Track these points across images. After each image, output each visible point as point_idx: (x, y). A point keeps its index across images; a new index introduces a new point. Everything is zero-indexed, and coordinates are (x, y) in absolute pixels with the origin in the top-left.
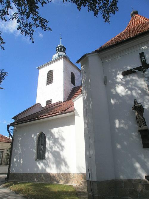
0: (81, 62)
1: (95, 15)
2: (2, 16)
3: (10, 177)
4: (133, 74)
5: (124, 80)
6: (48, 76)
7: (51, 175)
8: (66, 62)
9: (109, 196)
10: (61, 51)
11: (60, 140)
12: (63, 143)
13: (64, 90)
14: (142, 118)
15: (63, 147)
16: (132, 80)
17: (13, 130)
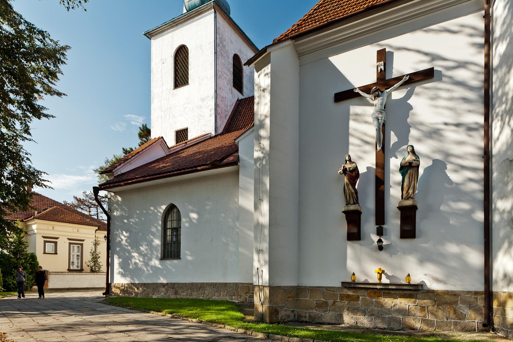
8: (222, 23)
9: (286, 308)
14: (353, 191)
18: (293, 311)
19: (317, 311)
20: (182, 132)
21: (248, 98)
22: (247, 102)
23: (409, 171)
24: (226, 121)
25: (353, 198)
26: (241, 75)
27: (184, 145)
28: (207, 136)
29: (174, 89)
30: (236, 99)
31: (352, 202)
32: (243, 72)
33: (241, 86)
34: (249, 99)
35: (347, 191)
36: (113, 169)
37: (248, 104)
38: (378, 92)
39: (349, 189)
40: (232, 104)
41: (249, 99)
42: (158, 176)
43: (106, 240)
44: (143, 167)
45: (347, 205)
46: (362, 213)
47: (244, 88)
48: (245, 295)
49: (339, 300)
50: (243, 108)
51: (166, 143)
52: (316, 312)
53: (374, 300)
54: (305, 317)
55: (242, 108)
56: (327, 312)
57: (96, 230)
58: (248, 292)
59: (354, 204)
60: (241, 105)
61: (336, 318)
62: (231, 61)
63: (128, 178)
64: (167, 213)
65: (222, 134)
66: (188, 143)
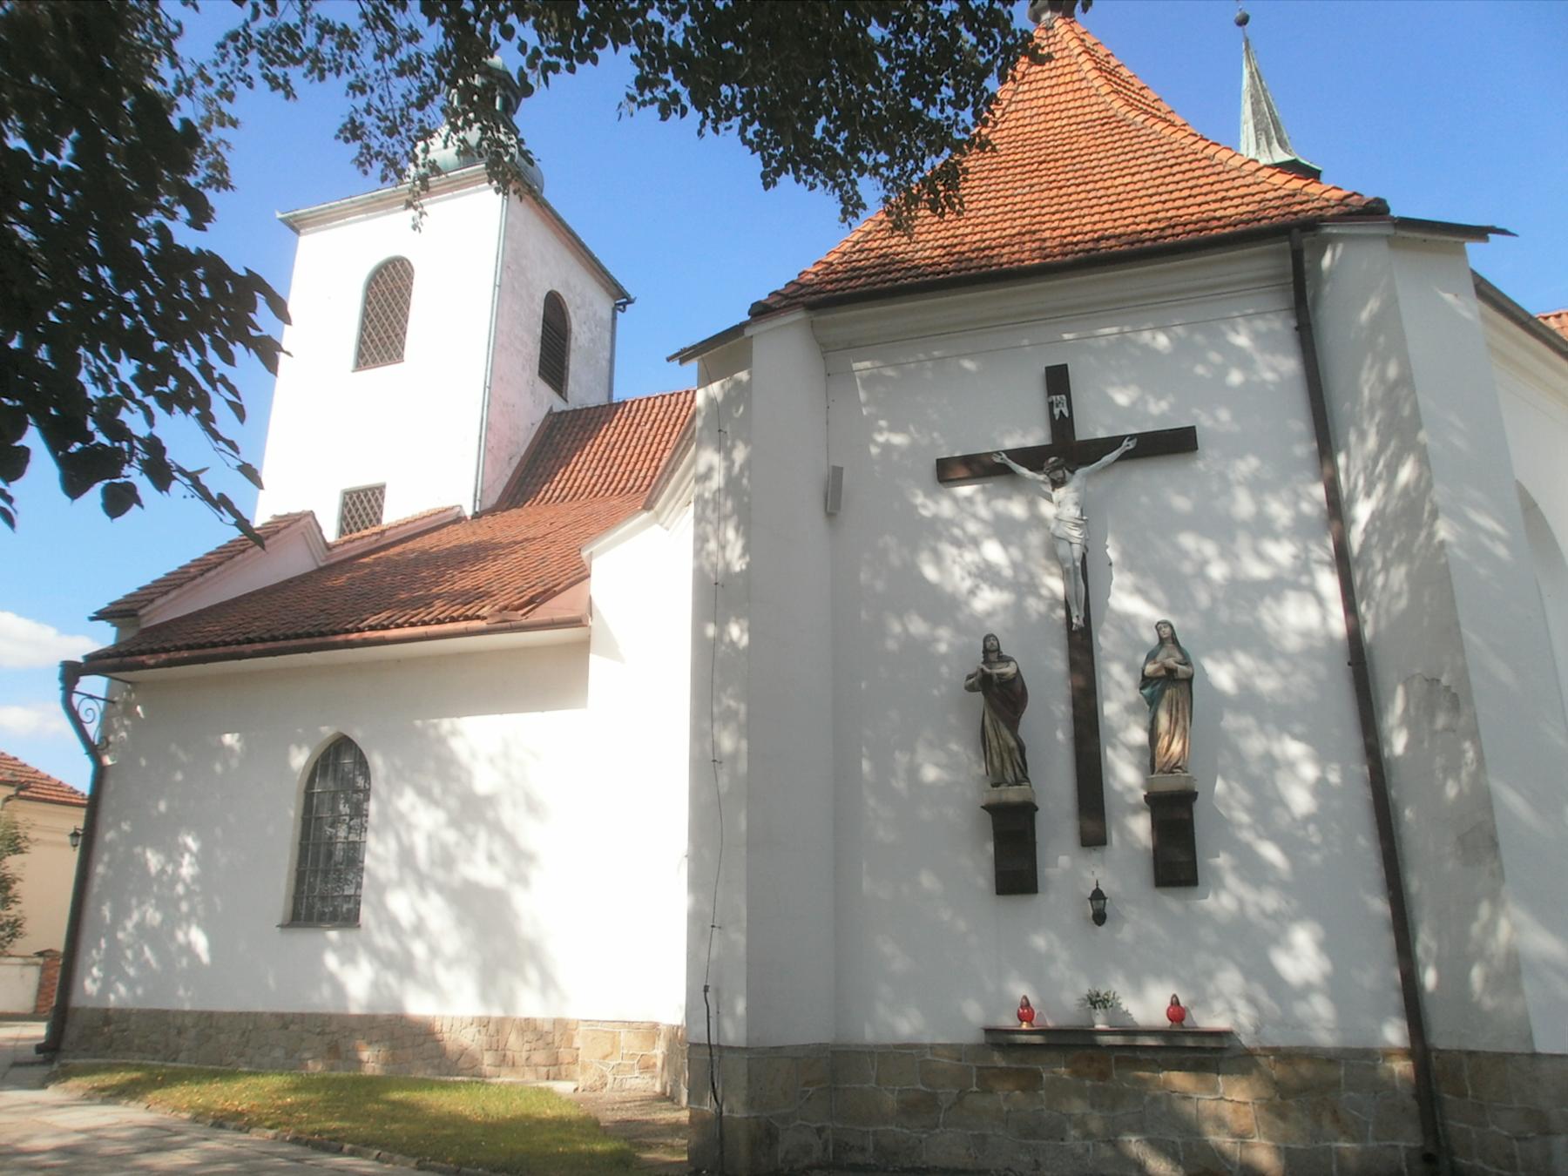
0: (699, 361)
1: (844, 220)
2: (272, 62)
3: (72, 1033)
4: (1003, 478)
6: (367, 301)
8: (523, 210)
9: (799, 1122)
11: (509, 815)
12: (529, 834)
13: (489, 428)
14: (1013, 743)
15: (521, 857)
17: (102, 703)
18: (820, 1131)
19: (902, 1127)
20: (366, 495)
21: (582, 410)
22: (580, 423)
23: (1168, 692)
24: (510, 473)
25: (1012, 763)
26: (565, 346)
27: (374, 538)
29: (353, 371)
30: (546, 410)
31: (1009, 776)
34: (587, 414)
35: (994, 744)
36: (141, 608)
37: (581, 427)
40: (533, 424)
41: (587, 414)
42: (307, 641)
43: (78, 848)
45: (994, 785)
46: (1037, 809)
48: (600, 1063)
49: (975, 1089)
51: (320, 531)
52: (899, 1130)
53: (1088, 1083)
54: (863, 1150)
56: (938, 1131)
57: (8, 799)
58: (612, 1053)
59: (1018, 783)
60: (560, 429)
61: (968, 1149)
65: (492, 511)
66: (387, 534)
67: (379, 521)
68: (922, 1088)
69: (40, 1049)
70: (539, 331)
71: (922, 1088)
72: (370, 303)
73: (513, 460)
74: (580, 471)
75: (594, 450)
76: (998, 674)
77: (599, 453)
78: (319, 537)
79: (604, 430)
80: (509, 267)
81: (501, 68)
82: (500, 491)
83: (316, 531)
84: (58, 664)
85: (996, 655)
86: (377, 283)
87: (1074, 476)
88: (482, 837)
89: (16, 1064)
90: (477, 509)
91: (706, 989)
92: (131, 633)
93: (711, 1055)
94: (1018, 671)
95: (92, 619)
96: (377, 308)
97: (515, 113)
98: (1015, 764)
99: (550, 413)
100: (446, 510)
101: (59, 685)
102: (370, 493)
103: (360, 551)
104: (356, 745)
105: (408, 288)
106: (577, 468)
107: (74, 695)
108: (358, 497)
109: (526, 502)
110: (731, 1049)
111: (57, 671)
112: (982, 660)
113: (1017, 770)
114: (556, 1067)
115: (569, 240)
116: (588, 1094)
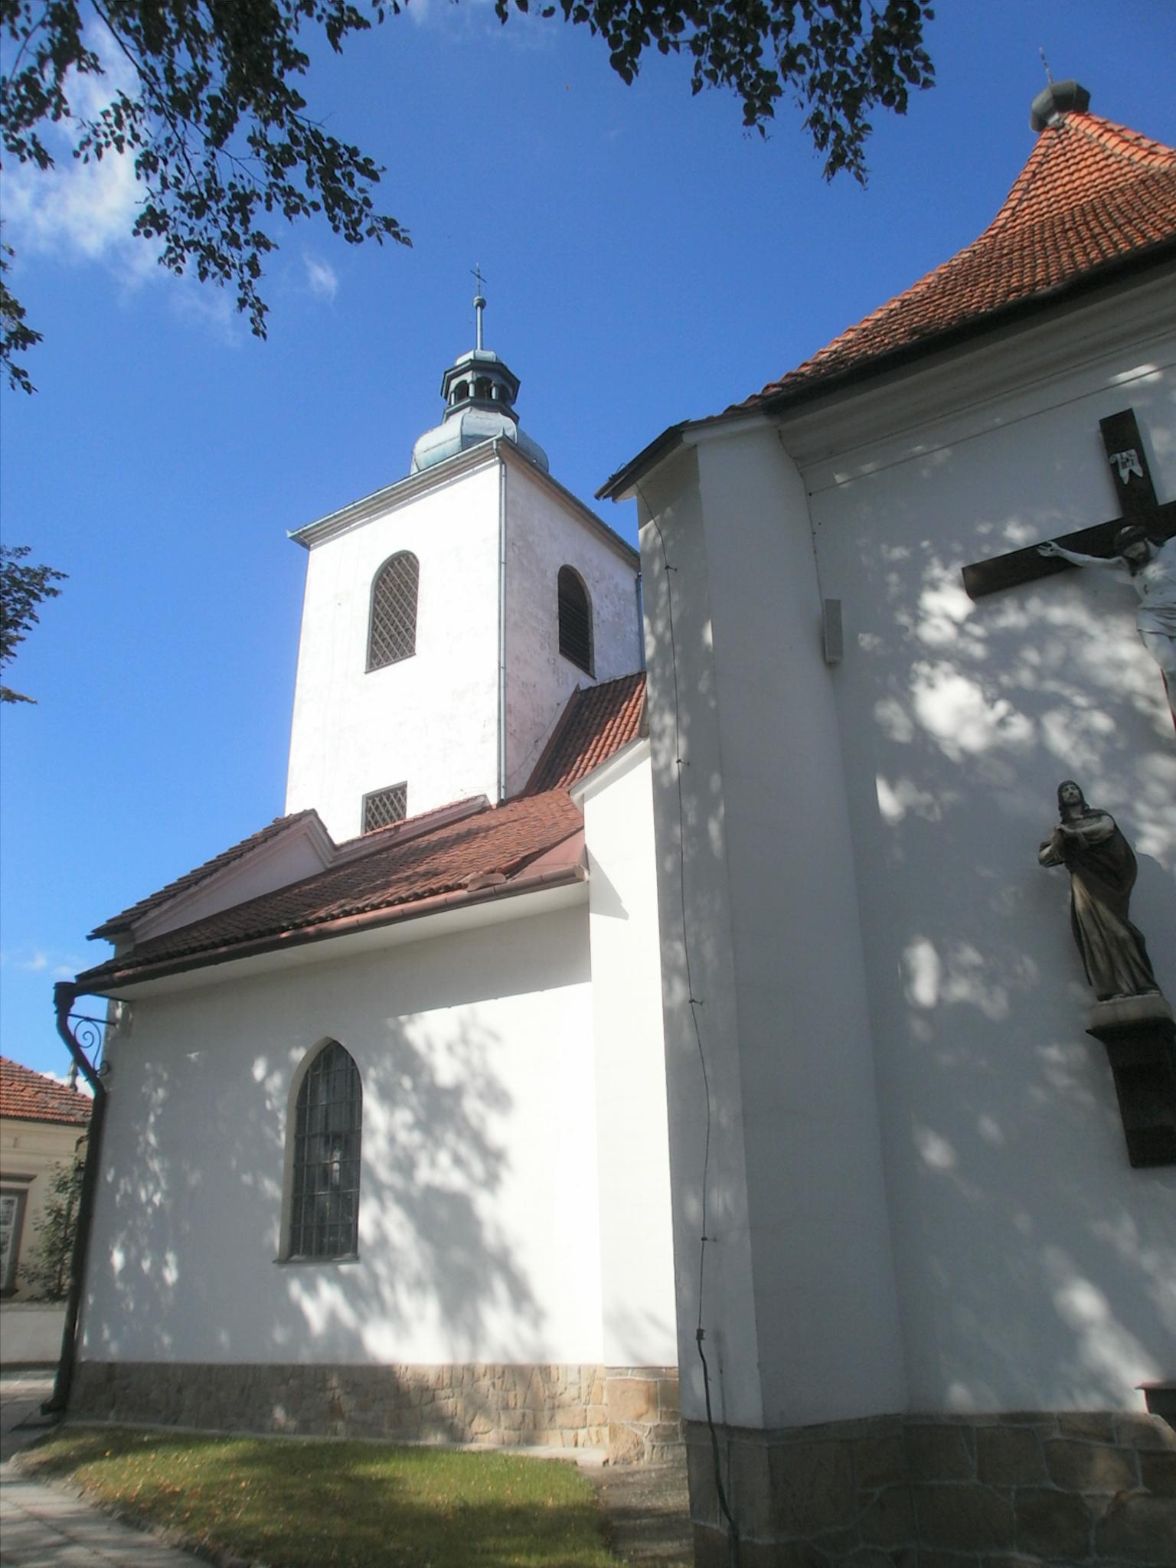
3: (78, 1390)
5: (977, 630)
6: (375, 601)
7: (406, 1379)
10: (483, 401)
12: (498, 1130)
14: (1123, 933)
16: (1041, 633)
17: (102, 1027)
20: (388, 798)
21: (610, 684)
22: (609, 697)
24: (537, 756)
25: (1127, 964)
27: (388, 834)
28: (470, 804)
29: (366, 673)
30: (572, 690)
32: (591, 614)
33: (588, 651)
34: (615, 686)
35: (1095, 937)
36: (134, 921)
37: (610, 700)
38: (1146, 545)
39: (1098, 922)
40: (558, 704)
41: (615, 686)
44: (241, 912)
47: (596, 657)
48: (634, 1426)
50: (595, 712)
51: (325, 830)
55: (591, 712)
59: (1140, 990)
62: (553, 584)
63: (176, 949)
64: (309, 1076)
66: (402, 829)
67: (400, 817)
68: (1053, 1486)
69: (47, 1408)
70: (555, 607)
71: (1053, 1486)
72: (379, 603)
73: (539, 743)
74: (611, 745)
75: (625, 721)
76: (1085, 834)
77: (630, 724)
78: (324, 837)
79: (634, 700)
80: (513, 544)
81: (494, 360)
82: (527, 776)
83: (321, 831)
84: (53, 986)
85: (1079, 808)
86: (384, 581)
87: (1163, 550)
88: (450, 1137)
89: (22, 1427)
90: (502, 797)
91: (700, 1335)
92: (130, 948)
93: (714, 1439)
94: (1115, 826)
95: (90, 938)
96: (386, 607)
97: (514, 403)
98: (1133, 965)
99: (577, 691)
100: (468, 800)
101: (54, 1008)
102: (392, 795)
103: (372, 850)
104: (347, 1052)
105: (415, 582)
106: (608, 742)
107: (70, 1018)
108: (381, 800)
109: (555, 785)
110: (742, 1430)
111: (51, 994)
112: (1060, 819)
113: (1136, 971)
114: (585, 1430)
115: (578, 512)
116: (619, 1469)
